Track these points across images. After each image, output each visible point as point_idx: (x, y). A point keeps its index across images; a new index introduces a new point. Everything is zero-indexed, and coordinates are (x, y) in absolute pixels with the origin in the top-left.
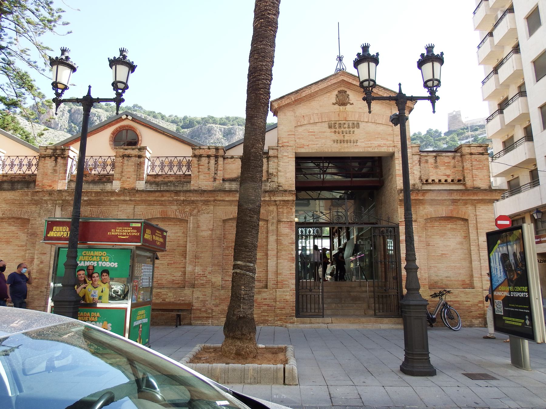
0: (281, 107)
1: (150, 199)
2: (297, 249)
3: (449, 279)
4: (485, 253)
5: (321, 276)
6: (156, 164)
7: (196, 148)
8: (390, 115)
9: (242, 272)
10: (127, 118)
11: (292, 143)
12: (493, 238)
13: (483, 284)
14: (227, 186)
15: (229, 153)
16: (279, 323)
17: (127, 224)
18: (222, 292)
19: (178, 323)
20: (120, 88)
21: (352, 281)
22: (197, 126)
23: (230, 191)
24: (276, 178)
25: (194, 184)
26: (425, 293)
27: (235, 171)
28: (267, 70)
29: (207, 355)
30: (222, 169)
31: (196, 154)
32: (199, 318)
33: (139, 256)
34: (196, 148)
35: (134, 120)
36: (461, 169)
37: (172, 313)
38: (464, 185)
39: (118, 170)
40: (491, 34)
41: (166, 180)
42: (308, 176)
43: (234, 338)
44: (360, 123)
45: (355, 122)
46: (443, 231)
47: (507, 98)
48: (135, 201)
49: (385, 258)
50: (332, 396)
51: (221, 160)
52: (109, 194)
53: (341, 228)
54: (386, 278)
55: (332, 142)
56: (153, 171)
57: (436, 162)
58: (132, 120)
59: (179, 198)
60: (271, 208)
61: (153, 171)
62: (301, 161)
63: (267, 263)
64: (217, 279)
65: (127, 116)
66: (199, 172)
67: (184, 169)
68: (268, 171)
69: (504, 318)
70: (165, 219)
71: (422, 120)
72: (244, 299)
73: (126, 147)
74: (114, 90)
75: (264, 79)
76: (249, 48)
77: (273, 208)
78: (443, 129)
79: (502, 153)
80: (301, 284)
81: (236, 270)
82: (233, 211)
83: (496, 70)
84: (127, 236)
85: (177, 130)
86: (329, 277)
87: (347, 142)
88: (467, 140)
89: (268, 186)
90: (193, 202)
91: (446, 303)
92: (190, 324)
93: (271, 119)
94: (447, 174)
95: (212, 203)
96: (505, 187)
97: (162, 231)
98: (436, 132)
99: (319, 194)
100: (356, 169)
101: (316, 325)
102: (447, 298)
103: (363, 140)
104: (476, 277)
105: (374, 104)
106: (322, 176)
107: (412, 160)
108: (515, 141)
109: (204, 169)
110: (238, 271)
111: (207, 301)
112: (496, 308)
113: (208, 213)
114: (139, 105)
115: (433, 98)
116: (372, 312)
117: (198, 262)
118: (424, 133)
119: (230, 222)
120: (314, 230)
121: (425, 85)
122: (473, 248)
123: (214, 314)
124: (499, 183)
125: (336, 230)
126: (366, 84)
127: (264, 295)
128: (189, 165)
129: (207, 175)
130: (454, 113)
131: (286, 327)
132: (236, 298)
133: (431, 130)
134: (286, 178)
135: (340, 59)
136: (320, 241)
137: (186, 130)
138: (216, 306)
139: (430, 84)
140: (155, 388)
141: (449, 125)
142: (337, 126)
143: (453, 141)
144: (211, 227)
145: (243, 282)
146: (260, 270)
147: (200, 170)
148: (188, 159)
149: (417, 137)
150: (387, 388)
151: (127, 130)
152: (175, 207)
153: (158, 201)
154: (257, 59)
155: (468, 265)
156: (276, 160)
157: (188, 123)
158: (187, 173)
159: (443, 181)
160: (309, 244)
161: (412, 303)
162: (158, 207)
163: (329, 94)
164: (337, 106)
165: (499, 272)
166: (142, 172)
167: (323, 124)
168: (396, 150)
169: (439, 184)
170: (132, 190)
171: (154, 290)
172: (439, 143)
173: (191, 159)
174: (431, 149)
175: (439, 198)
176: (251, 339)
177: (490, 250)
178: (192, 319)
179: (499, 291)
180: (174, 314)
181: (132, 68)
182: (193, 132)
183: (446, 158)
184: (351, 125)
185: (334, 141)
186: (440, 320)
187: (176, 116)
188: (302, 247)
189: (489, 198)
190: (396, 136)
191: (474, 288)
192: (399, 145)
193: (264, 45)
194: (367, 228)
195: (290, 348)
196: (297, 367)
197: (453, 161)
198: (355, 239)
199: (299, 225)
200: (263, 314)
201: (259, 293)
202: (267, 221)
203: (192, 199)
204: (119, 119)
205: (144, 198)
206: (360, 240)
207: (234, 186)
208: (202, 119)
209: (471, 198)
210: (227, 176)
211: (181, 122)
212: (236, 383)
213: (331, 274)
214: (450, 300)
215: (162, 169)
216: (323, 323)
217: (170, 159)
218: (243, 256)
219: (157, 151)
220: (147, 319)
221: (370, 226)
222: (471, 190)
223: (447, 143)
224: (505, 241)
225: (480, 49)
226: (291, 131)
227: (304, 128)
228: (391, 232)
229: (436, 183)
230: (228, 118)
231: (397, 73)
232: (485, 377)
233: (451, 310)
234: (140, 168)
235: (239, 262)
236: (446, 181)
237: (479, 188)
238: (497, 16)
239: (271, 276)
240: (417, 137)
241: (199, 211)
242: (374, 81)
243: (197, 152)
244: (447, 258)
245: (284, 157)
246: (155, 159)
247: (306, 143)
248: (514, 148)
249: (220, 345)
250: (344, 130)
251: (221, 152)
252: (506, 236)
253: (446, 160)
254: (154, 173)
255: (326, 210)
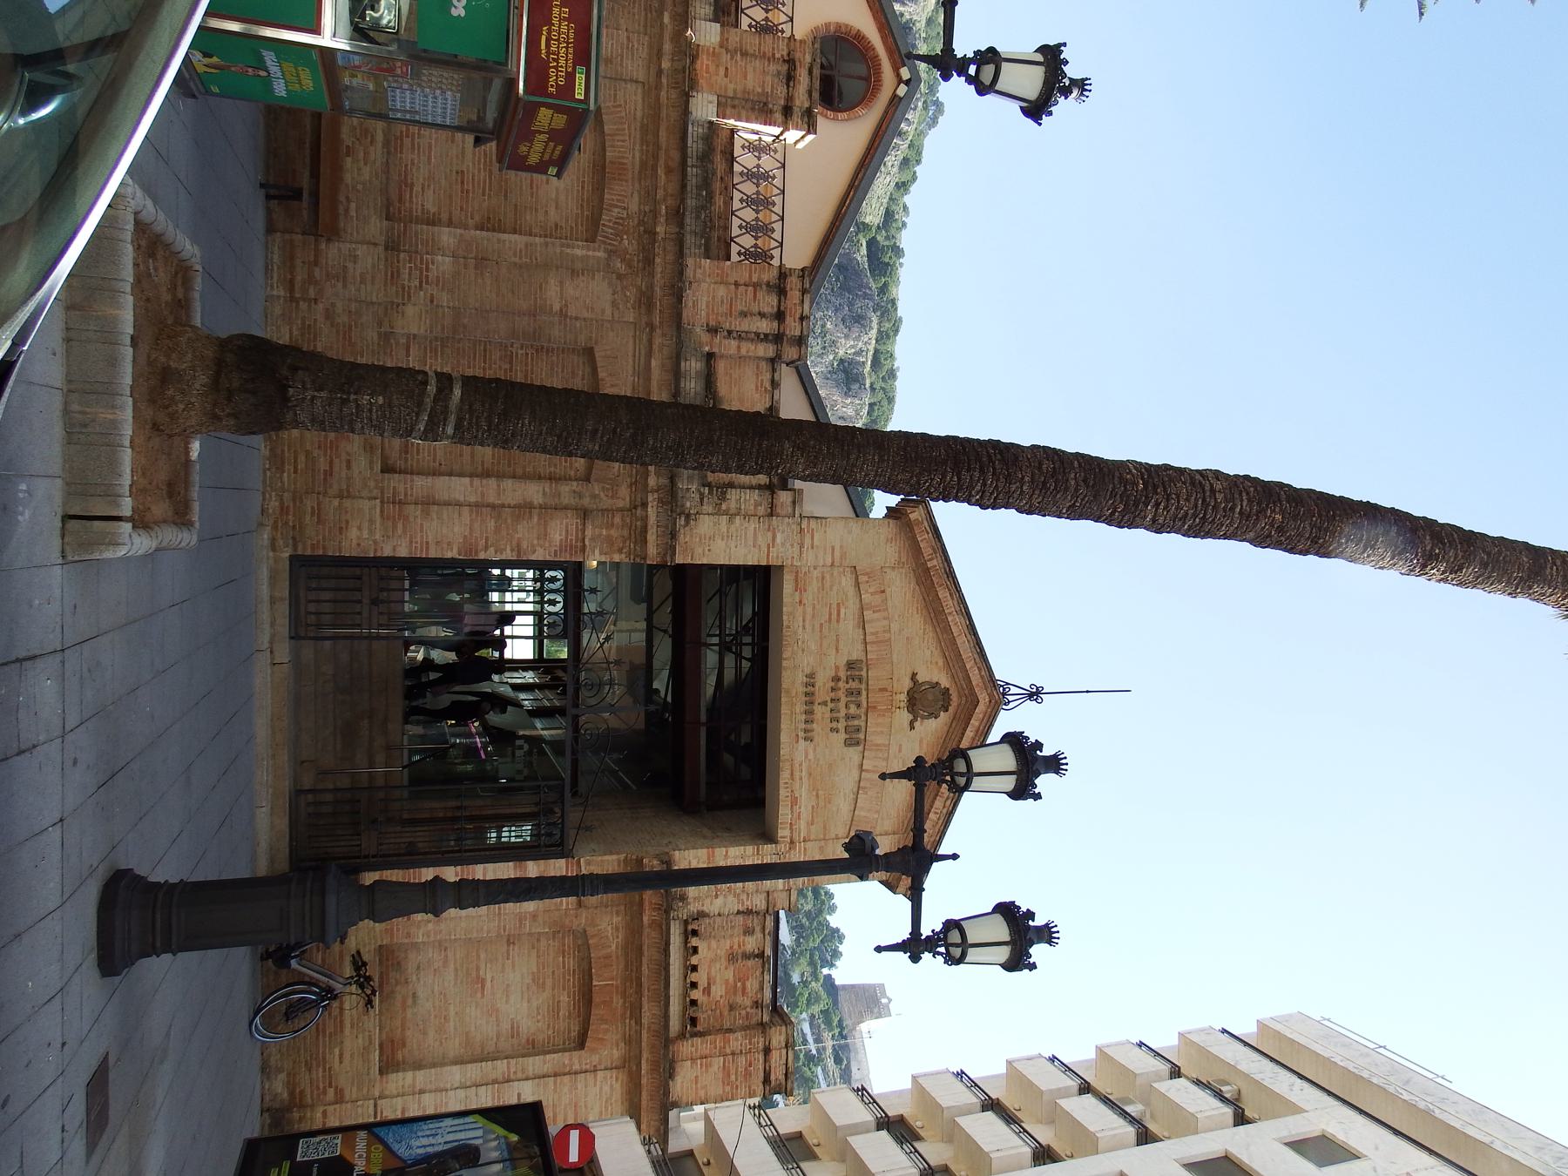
0: (912, 530)
1: (663, 134)
2: (504, 565)
3: (410, 1001)
4: (486, 1099)
5: (421, 632)
6: (765, 157)
7: (807, 281)
8: (876, 831)
9: (428, 401)
10: (900, 81)
11: (809, 557)
12: (524, 1121)
13: (406, 1095)
14: (693, 366)
15: (788, 378)
16: (274, 504)
17: (582, 56)
18: (372, 335)
19: (272, 192)
20: (984, 70)
21: (406, 722)
22: (873, 285)
23: (677, 374)
24: (710, 510)
25: (700, 268)
26: (366, 935)
27: (735, 390)
28: (1009, 494)
29: (162, 276)
30: (743, 352)
31: (789, 280)
32: (289, 259)
33: (488, 85)
34: (807, 281)
35: (895, 100)
36: (727, 1025)
37: (307, 174)
38: (682, 1036)
39: (752, 43)
40: (1085, 1088)
41: (717, 186)
42: (716, 600)
43: (219, 366)
44: (860, 748)
45: (862, 736)
46: (549, 982)
47: (918, 1138)
48: (658, 86)
49: (471, 819)
50: (28, 664)
51: (768, 350)
52: (680, 10)
53: (564, 693)
54: (413, 822)
55: (807, 671)
56: (743, 147)
57: (746, 956)
58: (895, 96)
59: (662, 220)
60: (624, 491)
61: (743, 147)
62: (759, 581)
63: (461, 475)
64: (412, 320)
65: (907, 83)
66: (736, 284)
67: (747, 241)
68: (731, 485)
69: (286, 1165)
70: (601, 171)
71: (864, 911)
72: (345, 402)
73: (817, 72)
74: (977, 53)
75: (984, 484)
76: (1070, 448)
77: (624, 496)
78: (844, 973)
79: (770, 1132)
80: (395, 573)
81: (433, 381)
82: (619, 381)
83: (991, 1105)
84: (548, 53)
85: (865, 227)
86: (420, 657)
87: (809, 712)
88: (810, 1039)
89: (689, 485)
90: (649, 262)
91: (335, 997)
92: (270, 229)
93: (882, 502)
94: (713, 988)
95: (644, 319)
96: (675, 1146)
97: (561, 163)
98: (836, 954)
99: (665, 631)
100: (733, 737)
101: (265, 616)
102: (351, 1000)
103: (811, 756)
104: (414, 1079)
105: (904, 788)
106: (715, 640)
107: (752, 894)
108: (804, 1165)
109: (745, 300)
110: (432, 389)
111: (345, 286)
112: (318, 1139)
113: (614, 304)
114: (941, 119)
115: (914, 946)
116: (307, 782)
117: (466, 266)
118: (834, 920)
119: (588, 370)
120: (556, 614)
121: (951, 925)
122: (501, 1065)
123: (303, 305)
124: (689, 1128)
125: (559, 679)
126: (960, 766)
127: (361, 463)
128: (759, 256)
129: (724, 308)
130: (884, 1001)
131: (261, 525)
132: (349, 378)
133: (841, 938)
134: (712, 538)
135: (1035, 694)
136: (530, 631)
137: (864, 251)
138: (329, 315)
139: (955, 937)
140: (24, 113)
141: (852, 988)
142: (854, 685)
143: (808, 1000)
144: (572, 312)
145: (396, 402)
146: (440, 453)
147: (742, 288)
148: (776, 253)
149: (824, 903)
150: (55, 834)
151: (867, 79)
152: (634, 206)
153: (656, 157)
154: (1040, 468)
155: (451, 1054)
156: (761, 510)
157: (883, 260)
158: (734, 249)
159: (694, 977)
160: (518, 599)
161: (331, 901)
162: (637, 155)
163: (941, 663)
164: (907, 684)
165: (425, 1141)
166: (744, 113)
167: (860, 647)
168: (782, 847)
169: (686, 967)
170: (691, 79)
171: (380, 126)
172: (804, 961)
173: (775, 262)
174: (786, 937)
175: (645, 967)
176: (216, 418)
177: (488, 1113)
178: (287, 236)
179: (369, 1146)
180: (305, 182)
181: (1036, 110)
182: (858, 273)
183: (756, 984)
184: (856, 722)
185: (811, 676)
186: (284, 979)
187: (904, 225)
188: (511, 580)
189: (644, 1103)
190: (821, 848)
191: (381, 1072)
192: (796, 856)
193: (1076, 490)
194: (563, 766)
195: (187, 538)
196: (125, 559)
197: (748, 1002)
198: (534, 733)
199: (575, 572)
200: (302, 458)
201: (369, 448)
202: (587, 479)
203: (658, 260)
204: (903, 56)
205: (664, 113)
206: (526, 747)
207: (692, 387)
208: (893, 302)
209: (645, 1055)
210: (721, 367)
211: (887, 238)
212: (68, 366)
213: (427, 662)
214: (347, 1006)
215: (750, 175)
216: (273, 636)
217: (778, 200)
218: (477, 406)
219: (802, 158)
220: (284, 94)
221: (566, 775)
222: (666, 1055)
223: (805, 983)
224: (516, 1155)
225: (1049, 1064)
226: (843, 556)
227: (851, 591)
228: (550, 835)
229: (686, 959)
230: (892, 374)
231: (988, 849)
232: (97, 1121)
233: (313, 1011)
234: (753, 109)
235: (457, 392)
236: (694, 985)
237: (671, 1076)
238: (1131, 1102)
239: (421, 484)
240: (823, 903)
241: (620, 277)
242: (966, 788)
243: (793, 283)
244: (473, 993)
245: (770, 534)
246: (779, 156)
247: (809, 597)
248: (782, 1163)
249: (197, 321)
250: (842, 705)
251: (790, 352)
252: (531, 1158)
253: (752, 985)
254: (737, 151)
255: (619, 649)
